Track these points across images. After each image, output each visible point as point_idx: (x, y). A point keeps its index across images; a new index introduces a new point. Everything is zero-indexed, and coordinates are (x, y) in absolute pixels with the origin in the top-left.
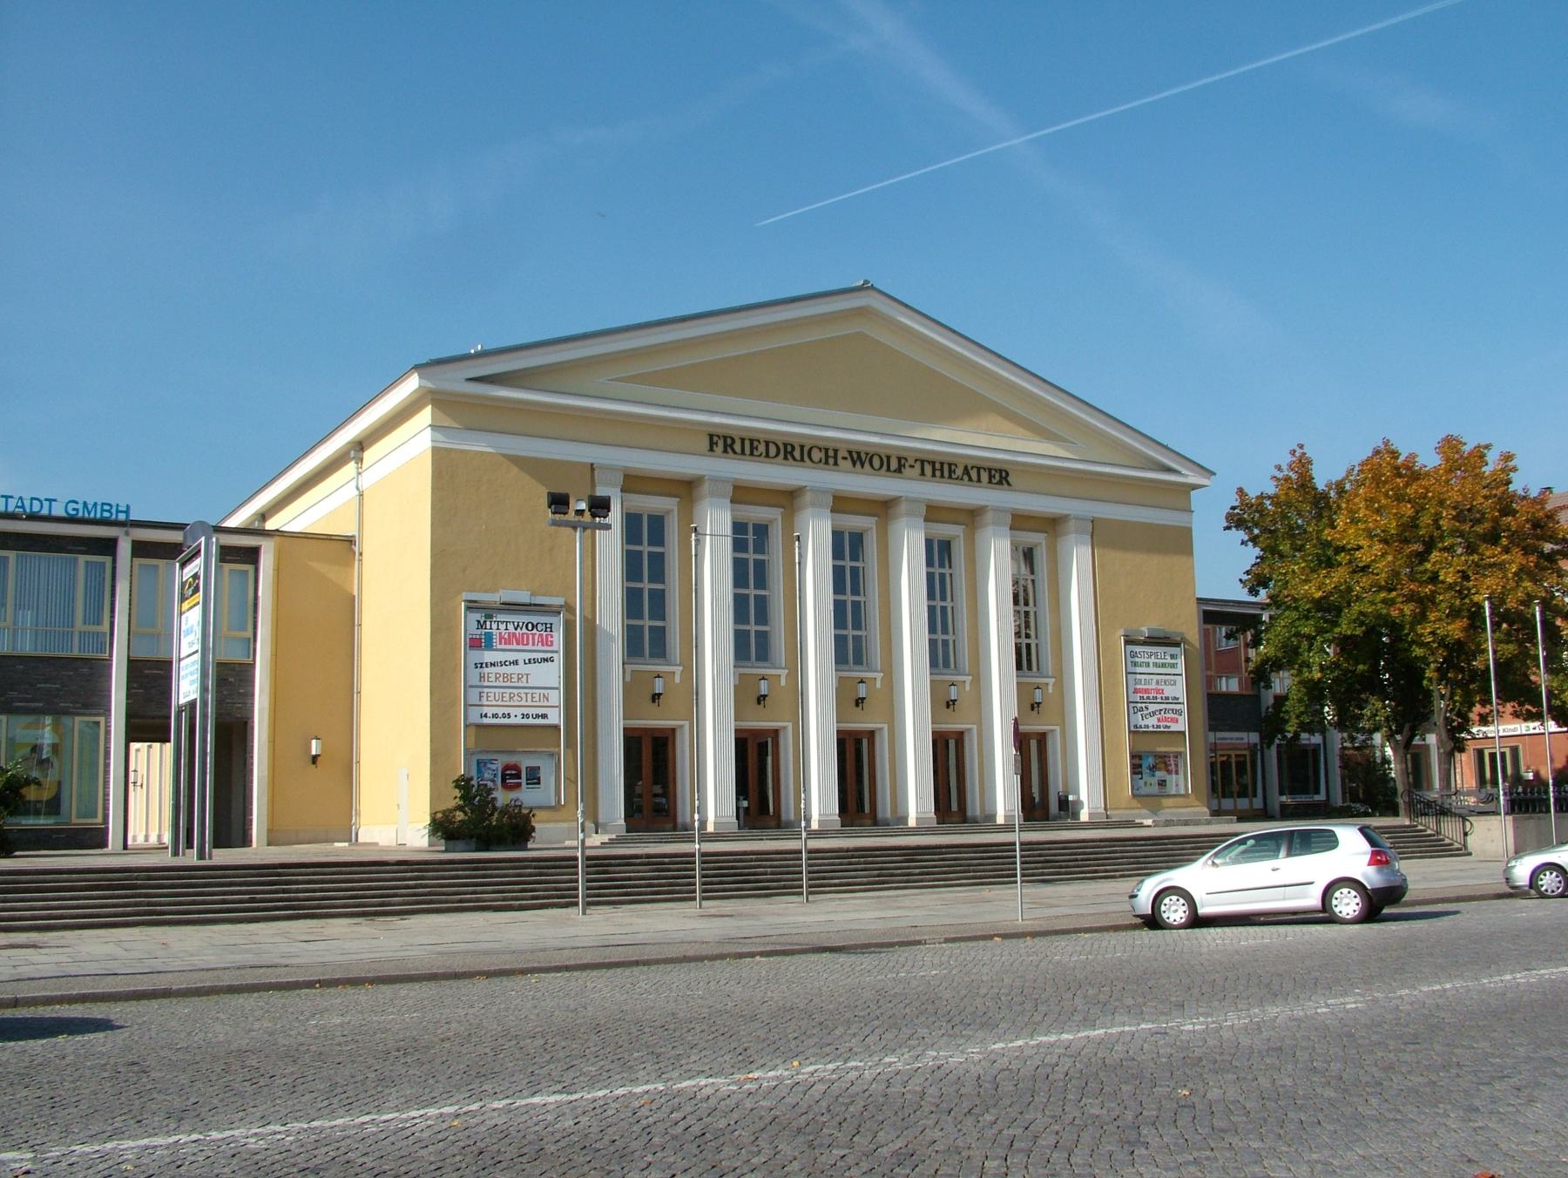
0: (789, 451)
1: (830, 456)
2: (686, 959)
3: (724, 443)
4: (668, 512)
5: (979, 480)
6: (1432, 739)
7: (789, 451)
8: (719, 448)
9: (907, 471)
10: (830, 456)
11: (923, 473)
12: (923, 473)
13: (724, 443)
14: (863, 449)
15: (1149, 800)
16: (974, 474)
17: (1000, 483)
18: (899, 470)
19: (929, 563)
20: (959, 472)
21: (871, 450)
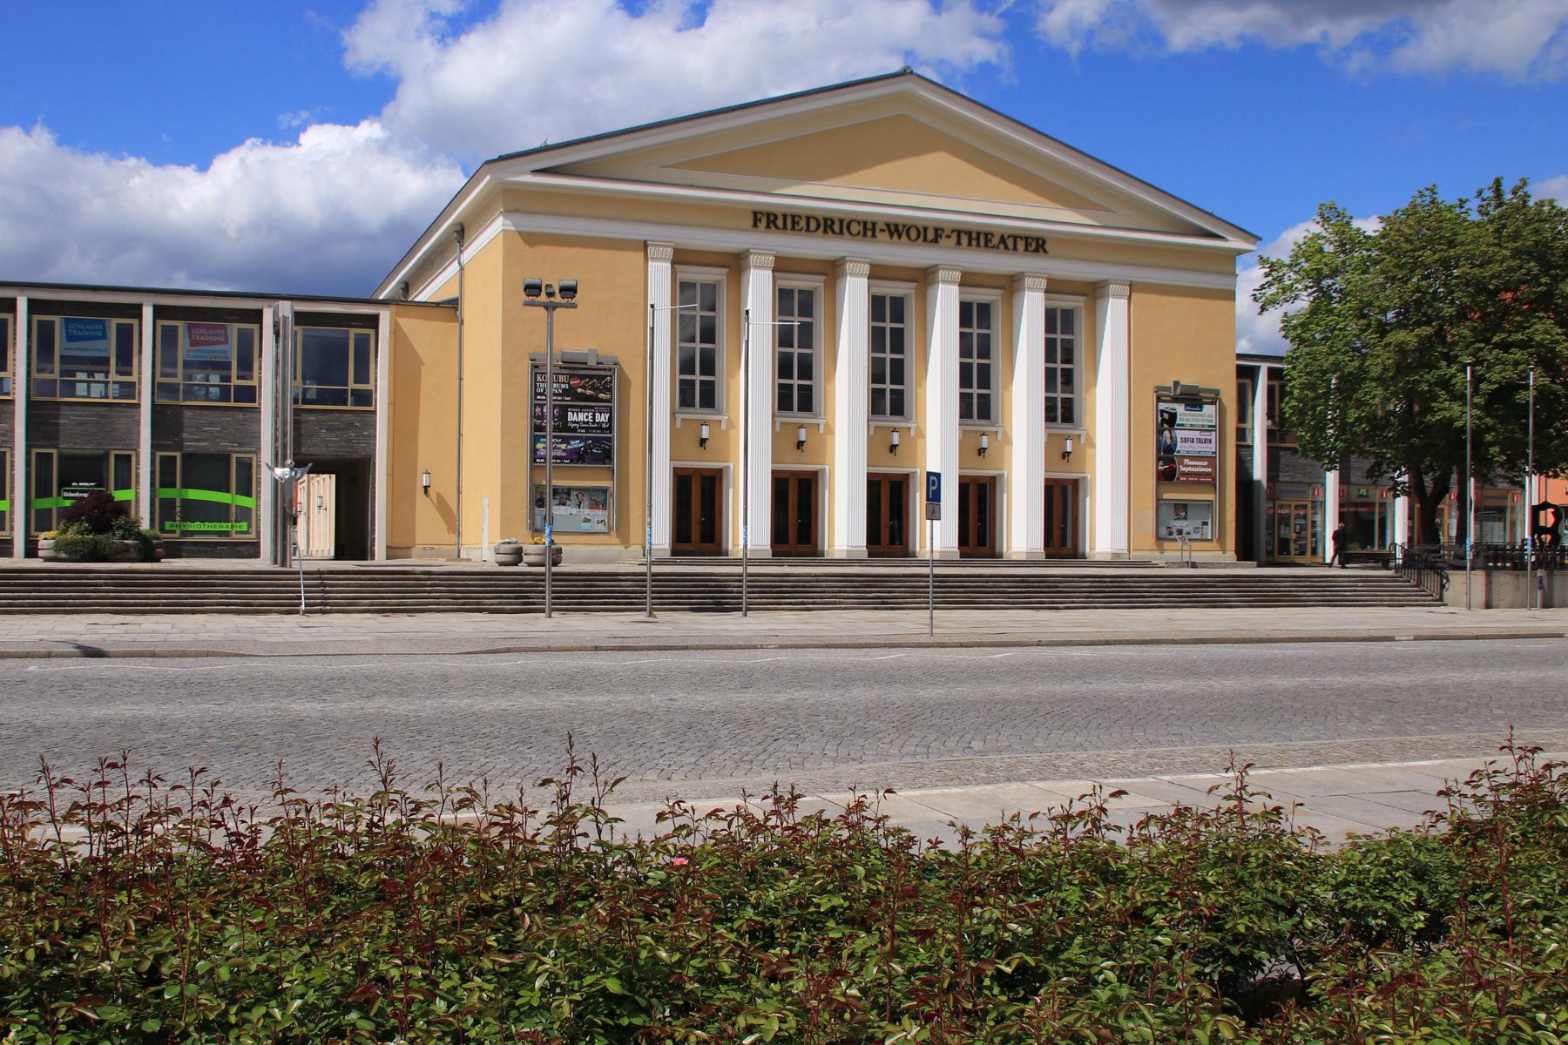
3: (767, 220)
5: (1015, 248)
8: (762, 225)
9: (943, 241)
11: (959, 243)
12: (959, 243)
13: (767, 220)
16: (1010, 243)
17: (1037, 250)
18: (935, 241)
20: (995, 241)
21: (909, 223)
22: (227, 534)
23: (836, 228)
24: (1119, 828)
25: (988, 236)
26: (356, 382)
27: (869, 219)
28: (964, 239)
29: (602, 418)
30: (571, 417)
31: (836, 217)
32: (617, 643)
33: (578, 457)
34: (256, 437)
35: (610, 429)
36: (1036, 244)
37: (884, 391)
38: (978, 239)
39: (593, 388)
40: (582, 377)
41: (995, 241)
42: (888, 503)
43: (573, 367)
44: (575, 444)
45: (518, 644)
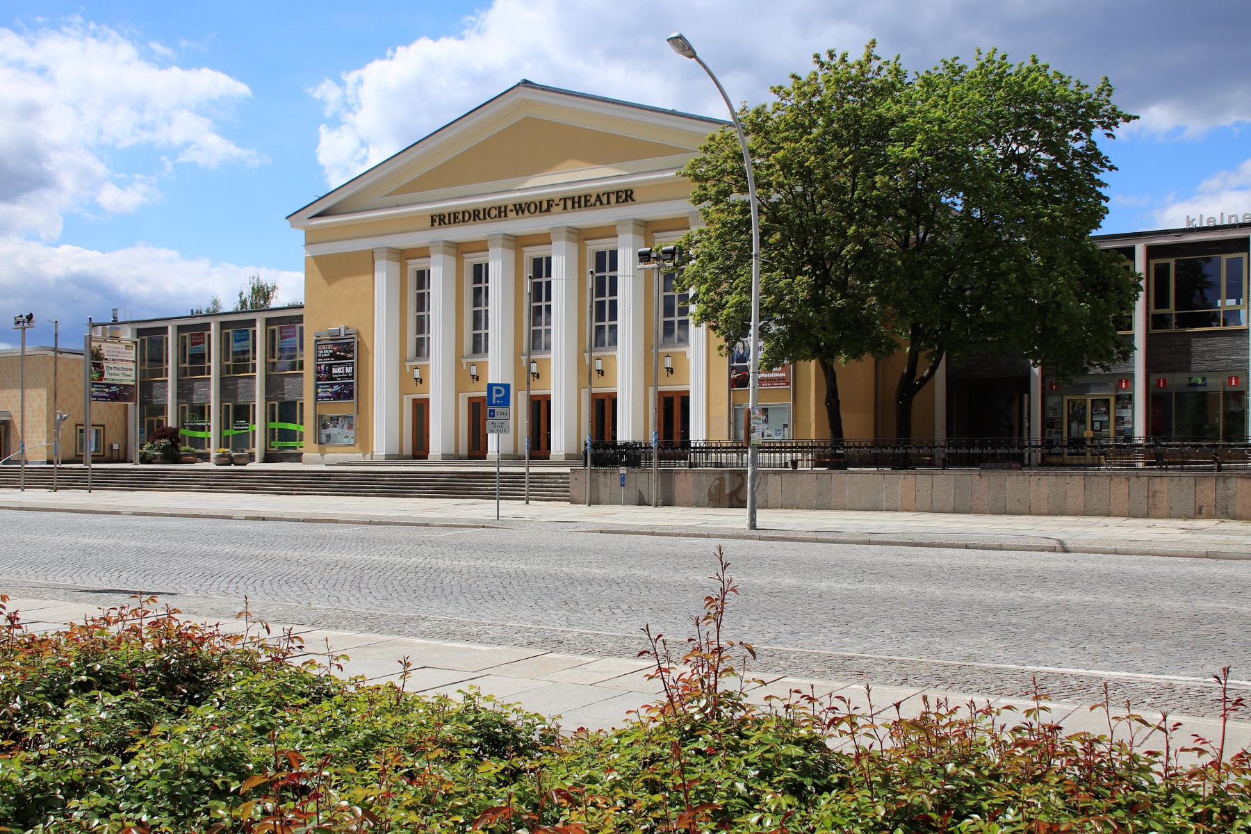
0: (476, 215)
1: (502, 212)
2: (145, 514)
3: (439, 220)
4: (363, 440)
5: (608, 203)
6: (234, 688)
7: (476, 215)
8: (436, 224)
9: (554, 209)
10: (502, 212)
11: (565, 208)
12: (565, 208)
13: (439, 220)
14: (523, 201)
15: (1072, 404)
16: (604, 199)
17: (626, 200)
18: (548, 210)
19: (549, 284)
20: (593, 200)
21: (529, 200)
22: (294, 448)
23: (481, 216)
24: (925, 698)
25: (587, 198)
26: (1167, 265)
27: (503, 204)
28: (569, 203)
29: (349, 370)
30: (335, 371)
31: (481, 208)
32: (866, 538)
33: (337, 396)
34: (254, 391)
35: (352, 377)
36: (625, 196)
37: (680, 315)
38: (579, 202)
39: (345, 351)
40: (339, 344)
41: (593, 200)
42: (480, 414)
43: (334, 337)
44: (336, 388)
45: (781, 535)
